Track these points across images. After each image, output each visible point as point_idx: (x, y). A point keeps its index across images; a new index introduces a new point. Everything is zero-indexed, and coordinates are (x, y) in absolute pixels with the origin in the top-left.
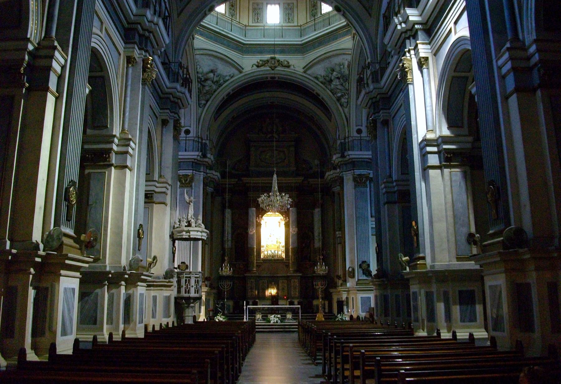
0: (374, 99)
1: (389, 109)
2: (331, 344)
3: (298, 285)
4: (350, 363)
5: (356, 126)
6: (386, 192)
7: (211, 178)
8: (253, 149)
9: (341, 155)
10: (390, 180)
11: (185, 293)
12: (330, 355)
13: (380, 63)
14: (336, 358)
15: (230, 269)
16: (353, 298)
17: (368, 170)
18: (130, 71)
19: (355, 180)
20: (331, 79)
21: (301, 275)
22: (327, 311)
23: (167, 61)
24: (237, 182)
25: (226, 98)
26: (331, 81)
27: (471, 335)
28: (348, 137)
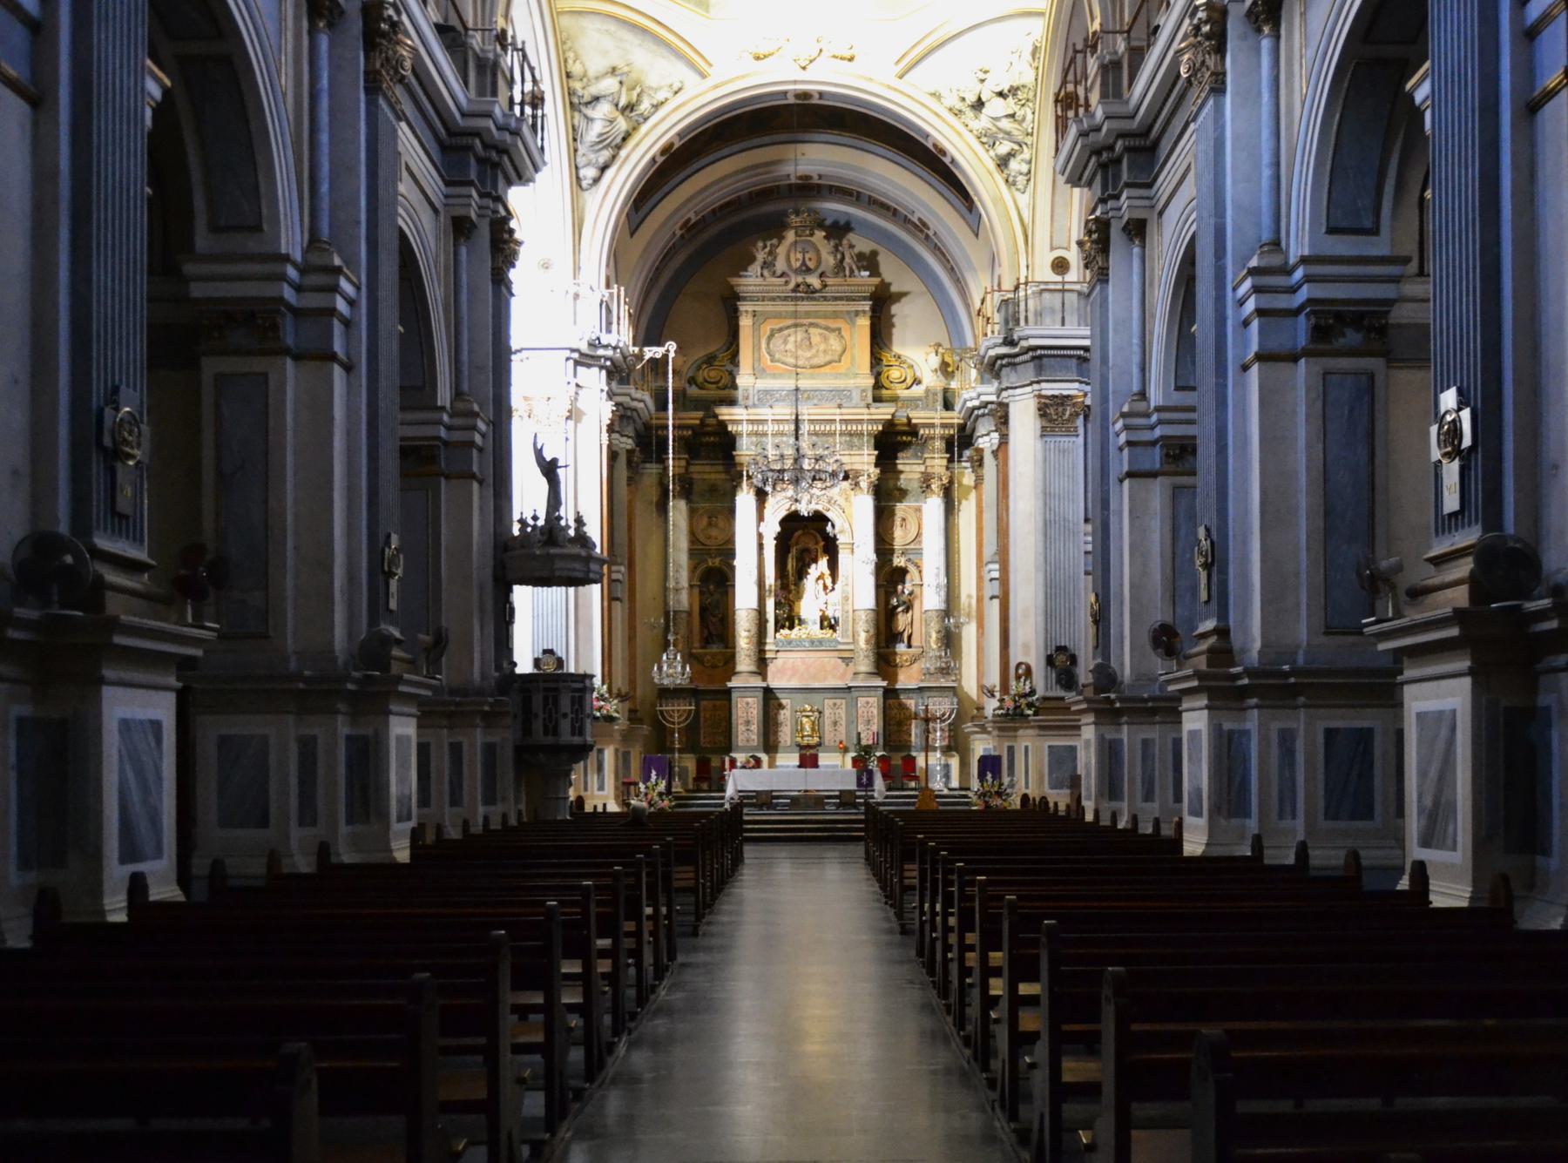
0: (1105, 155)
1: (1149, 186)
2: (950, 877)
3: (875, 712)
4: (978, 930)
5: (1052, 249)
6: (1129, 443)
7: (625, 409)
8: (745, 322)
9: (1005, 338)
10: (1141, 406)
11: (573, 734)
12: (933, 907)
13: (1128, 32)
14: (946, 915)
15: (684, 668)
16: (1026, 748)
17: (1081, 382)
18: (324, 42)
19: (1043, 411)
20: (980, 99)
21: (884, 684)
22: (774, 794)
23: (454, 21)
24: (702, 420)
25: (660, 160)
26: (979, 105)
27: (1354, 856)
28: (1026, 283)
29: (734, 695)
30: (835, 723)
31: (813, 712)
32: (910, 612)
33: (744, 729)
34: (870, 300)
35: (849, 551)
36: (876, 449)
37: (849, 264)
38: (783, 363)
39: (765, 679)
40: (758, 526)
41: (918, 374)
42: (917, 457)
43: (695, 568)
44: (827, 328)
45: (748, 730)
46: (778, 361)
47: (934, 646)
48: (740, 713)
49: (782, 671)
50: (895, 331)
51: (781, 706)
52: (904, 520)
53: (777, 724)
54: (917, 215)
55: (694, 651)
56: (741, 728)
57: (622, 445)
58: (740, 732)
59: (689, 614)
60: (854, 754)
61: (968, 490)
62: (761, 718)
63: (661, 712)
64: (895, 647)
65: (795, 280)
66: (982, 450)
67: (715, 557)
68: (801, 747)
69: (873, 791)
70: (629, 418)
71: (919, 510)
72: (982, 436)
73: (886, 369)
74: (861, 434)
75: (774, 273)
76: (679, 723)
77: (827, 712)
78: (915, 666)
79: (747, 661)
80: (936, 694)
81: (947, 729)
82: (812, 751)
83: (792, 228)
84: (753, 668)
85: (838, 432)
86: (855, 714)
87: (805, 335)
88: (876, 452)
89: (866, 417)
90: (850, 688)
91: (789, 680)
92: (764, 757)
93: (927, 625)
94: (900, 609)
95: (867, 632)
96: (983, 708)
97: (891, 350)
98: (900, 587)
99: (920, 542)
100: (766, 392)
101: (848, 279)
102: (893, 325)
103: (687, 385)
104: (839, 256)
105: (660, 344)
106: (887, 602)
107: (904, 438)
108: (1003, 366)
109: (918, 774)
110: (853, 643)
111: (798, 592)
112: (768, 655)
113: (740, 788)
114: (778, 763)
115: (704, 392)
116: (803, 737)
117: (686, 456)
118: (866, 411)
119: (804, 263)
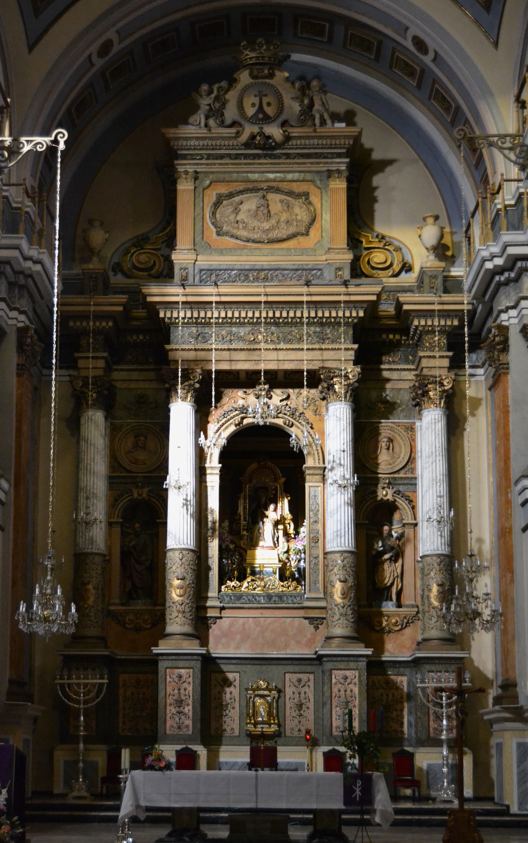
3: (356, 690)
15: (66, 609)
21: (369, 652)
29: (162, 665)
30: (300, 706)
31: (270, 690)
32: (400, 561)
33: (174, 711)
34: (347, 157)
35: (319, 478)
36: (354, 343)
37: (318, 111)
38: (232, 236)
39: (204, 642)
40: (197, 436)
41: (408, 258)
42: (407, 362)
43: (116, 500)
44: (290, 194)
45: (180, 713)
46: (226, 234)
47: (436, 603)
48: (169, 690)
49: (227, 635)
50: (377, 206)
51: (227, 683)
52: (391, 440)
53: (221, 707)
54: (413, 31)
55: (112, 608)
56: (171, 710)
57: (10, 322)
58: (169, 715)
59: (106, 559)
60: (326, 749)
61: (476, 403)
63: (62, 686)
64: (380, 606)
65: (249, 130)
66: (507, 328)
68: (253, 737)
69: (375, 811)
70: (22, 287)
71: (411, 429)
72: (508, 309)
73: (365, 252)
74: (335, 324)
75: (223, 122)
76: (86, 702)
77: (289, 691)
78: (408, 631)
79: (180, 619)
80: (440, 667)
81: (454, 716)
82: (268, 744)
83: (245, 66)
84: (187, 629)
85: (305, 320)
86: (327, 694)
87: (262, 201)
89: (342, 298)
90: (319, 659)
91: (238, 647)
92: (202, 751)
93: (424, 574)
94: (387, 556)
95: (344, 581)
96: (515, 685)
97: (372, 230)
98: (386, 528)
99: (413, 470)
100: (211, 271)
101: (319, 129)
102: (375, 200)
103: (111, 274)
104: (306, 101)
105: (46, 133)
106: (370, 546)
107: (391, 336)
108: (500, 285)
109: (416, 778)
110: (325, 599)
111: (252, 539)
112: (211, 613)
113: (143, 803)
114: (224, 757)
115: (132, 281)
116: (255, 724)
117: (105, 354)
118: (343, 289)
119: (261, 109)
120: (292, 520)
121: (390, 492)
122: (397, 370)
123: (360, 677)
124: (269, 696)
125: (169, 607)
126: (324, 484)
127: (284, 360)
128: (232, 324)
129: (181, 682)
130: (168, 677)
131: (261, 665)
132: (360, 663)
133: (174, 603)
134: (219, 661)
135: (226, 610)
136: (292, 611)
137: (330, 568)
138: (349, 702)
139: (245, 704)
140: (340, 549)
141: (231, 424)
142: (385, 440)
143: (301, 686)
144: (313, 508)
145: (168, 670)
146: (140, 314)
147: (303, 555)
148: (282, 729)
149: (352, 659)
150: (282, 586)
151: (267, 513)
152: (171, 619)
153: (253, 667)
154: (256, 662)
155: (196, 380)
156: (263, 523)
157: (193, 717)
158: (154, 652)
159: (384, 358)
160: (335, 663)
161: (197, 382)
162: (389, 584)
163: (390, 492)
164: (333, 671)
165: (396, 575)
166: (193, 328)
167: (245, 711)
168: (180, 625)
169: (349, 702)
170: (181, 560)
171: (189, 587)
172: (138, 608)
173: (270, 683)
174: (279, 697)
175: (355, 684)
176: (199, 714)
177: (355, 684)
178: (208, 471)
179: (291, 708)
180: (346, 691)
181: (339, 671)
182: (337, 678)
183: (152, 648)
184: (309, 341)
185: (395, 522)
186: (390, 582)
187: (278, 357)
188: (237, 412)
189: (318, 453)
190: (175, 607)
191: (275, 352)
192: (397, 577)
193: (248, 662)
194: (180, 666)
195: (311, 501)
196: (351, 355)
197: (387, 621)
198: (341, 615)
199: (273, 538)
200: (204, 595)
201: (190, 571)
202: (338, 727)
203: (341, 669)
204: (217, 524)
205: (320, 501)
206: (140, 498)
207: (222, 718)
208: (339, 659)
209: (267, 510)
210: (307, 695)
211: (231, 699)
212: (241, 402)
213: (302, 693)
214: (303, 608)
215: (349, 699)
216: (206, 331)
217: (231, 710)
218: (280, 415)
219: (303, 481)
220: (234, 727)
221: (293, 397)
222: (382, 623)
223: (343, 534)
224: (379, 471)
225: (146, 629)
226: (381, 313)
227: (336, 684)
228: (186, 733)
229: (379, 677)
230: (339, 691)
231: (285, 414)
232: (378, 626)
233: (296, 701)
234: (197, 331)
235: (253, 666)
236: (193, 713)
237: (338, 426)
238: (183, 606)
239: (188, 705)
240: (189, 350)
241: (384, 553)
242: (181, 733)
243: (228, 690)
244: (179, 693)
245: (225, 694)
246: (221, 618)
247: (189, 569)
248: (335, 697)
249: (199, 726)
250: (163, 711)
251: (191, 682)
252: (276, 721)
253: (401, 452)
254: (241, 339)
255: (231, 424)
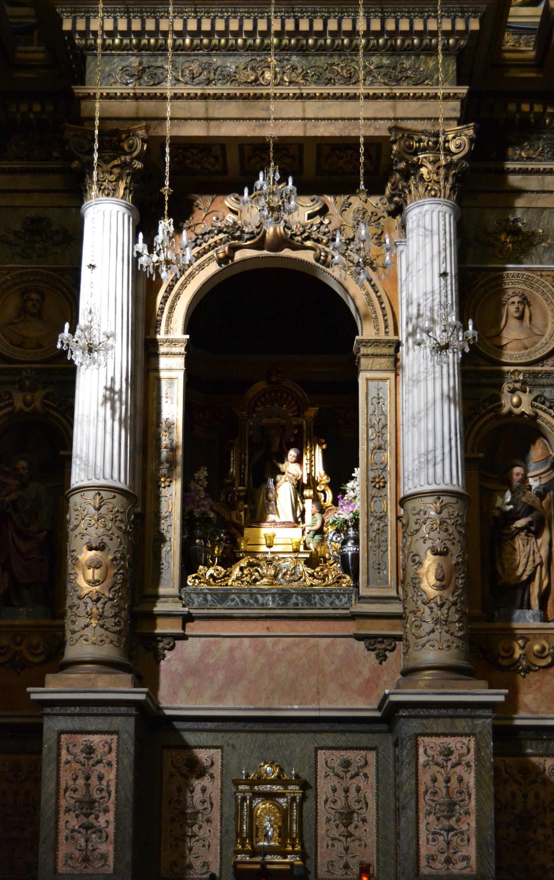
3: (471, 779)
31: (286, 784)
33: (74, 823)
35: (385, 362)
36: (460, 83)
45: (88, 827)
48: (66, 778)
62: (128, 793)
64: (510, 619)
67: (33, 389)
86: (408, 787)
88: (463, 90)
91: (218, 698)
94: (521, 523)
107: (525, 107)
120: (329, 485)
121: (526, 398)
122: (537, 172)
123: (478, 750)
124: (282, 795)
125: (71, 607)
126: (397, 375)
127: (317, 119)
128: (212, 49)
129: (91, 762)
130: (64, 752)
131: (267, 732)
132: (479, 722)
133: (80, 598)
134: (178, 725)
135: (196, 622)
136: (331, 623)
137: (413, 527)
138: (455, 804)
139: (233, 812)
140: (434, 487)
141: (210, 259)
142: (516, 299)
143: (349, 775)
144: (374, 421)
145: (63, 737)
146: (30, 56)
147: (351, 533)
148: (310, 864)
149: (461, 711)
150: (311, 575)
151: (282, 467)
152: (73, 632)
153: (250, 737)
154: (257, 727)
155: (135, 154)
156: (275, 483)
157: (116, 835)
158: (34, 697)
159: (510, 152)
160: (425, 721)
161: (138, 158)
162: (525, 577)
163: (526, 398)
164: (420, 739)
165: (538, 561)
166: (133, 59)
167: (232, 827)
168: (94, 644)
169: (455, 804)
170: (98, 509)
171: (113, 566)
172: (17, 622)
173: (286, 769)
174: (303, 798)
175: (468, 765)
176: (130, 829)
177: (468, 765)
178: (162, 349)
179: (328, 820)
180: (448, 781)
181: (434, 739)
182: (429, 752)
183: (29, 689)
184: (367, 83)
185: (532, 465)
186: (528, 573)
187: (304, 111)
188: (221, 236)
189: (385, 315)
190: (82, 606)
191: (299, 104)
192: (541, 564)
193: (240, 726)
194: (89, 728)
195: (371, 408)
196: (454, 110)
197: (522, 648)
198: (437, 621)
199: (294, 511)
200: (149, 591)
201: (117, 533)
202: (432, 858)
203: (438, 735)
204: (180, 453)
205: (388, 408)
206: (27, 410)
207: (184, 841)
208: (434, 712)
209: (283, 462)
210: (361, 793)
211: (203, 802)
212: (230, 218)
213: (353, 790)
214: (354, 617)
215: (456, 798)
216: (159, 64)
217: (204, 825)
218: (309, 243)
219: (355, 371)
220: (210, 859)
221: (334, 209)
222: (513, 653)
223: (439, 459)
224: (504, 360)
225: (35, 664)
226: (507, 55)
227: (426, 765)
228: (101, 871)
229: (507, 760)
230: (435, 780)
231: (318, 241)
232: (504, 658)
233: (339, 805)
234: (141, 64)
235: (249, 736)
236: (117, 828)
237: (428, 247)
238: (99, 605)
239: (106, 811)
240: (123, 97)
241: (514, 516)
242: (90, 871)
243: (198, 784)
244: (88, 786)
245: (192, 791)
246: (184, 637)
247: (114, 530)
248: (426, 792)
249: (128, 856)
250: (52, 824)
251: (114, 763)
252: (298, 848)
253: (546, 326)
254: (231, 78)
255: (210, 259)
